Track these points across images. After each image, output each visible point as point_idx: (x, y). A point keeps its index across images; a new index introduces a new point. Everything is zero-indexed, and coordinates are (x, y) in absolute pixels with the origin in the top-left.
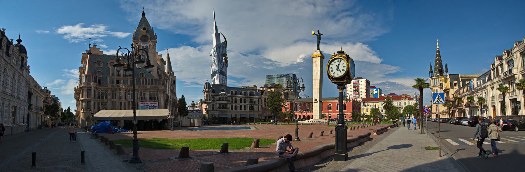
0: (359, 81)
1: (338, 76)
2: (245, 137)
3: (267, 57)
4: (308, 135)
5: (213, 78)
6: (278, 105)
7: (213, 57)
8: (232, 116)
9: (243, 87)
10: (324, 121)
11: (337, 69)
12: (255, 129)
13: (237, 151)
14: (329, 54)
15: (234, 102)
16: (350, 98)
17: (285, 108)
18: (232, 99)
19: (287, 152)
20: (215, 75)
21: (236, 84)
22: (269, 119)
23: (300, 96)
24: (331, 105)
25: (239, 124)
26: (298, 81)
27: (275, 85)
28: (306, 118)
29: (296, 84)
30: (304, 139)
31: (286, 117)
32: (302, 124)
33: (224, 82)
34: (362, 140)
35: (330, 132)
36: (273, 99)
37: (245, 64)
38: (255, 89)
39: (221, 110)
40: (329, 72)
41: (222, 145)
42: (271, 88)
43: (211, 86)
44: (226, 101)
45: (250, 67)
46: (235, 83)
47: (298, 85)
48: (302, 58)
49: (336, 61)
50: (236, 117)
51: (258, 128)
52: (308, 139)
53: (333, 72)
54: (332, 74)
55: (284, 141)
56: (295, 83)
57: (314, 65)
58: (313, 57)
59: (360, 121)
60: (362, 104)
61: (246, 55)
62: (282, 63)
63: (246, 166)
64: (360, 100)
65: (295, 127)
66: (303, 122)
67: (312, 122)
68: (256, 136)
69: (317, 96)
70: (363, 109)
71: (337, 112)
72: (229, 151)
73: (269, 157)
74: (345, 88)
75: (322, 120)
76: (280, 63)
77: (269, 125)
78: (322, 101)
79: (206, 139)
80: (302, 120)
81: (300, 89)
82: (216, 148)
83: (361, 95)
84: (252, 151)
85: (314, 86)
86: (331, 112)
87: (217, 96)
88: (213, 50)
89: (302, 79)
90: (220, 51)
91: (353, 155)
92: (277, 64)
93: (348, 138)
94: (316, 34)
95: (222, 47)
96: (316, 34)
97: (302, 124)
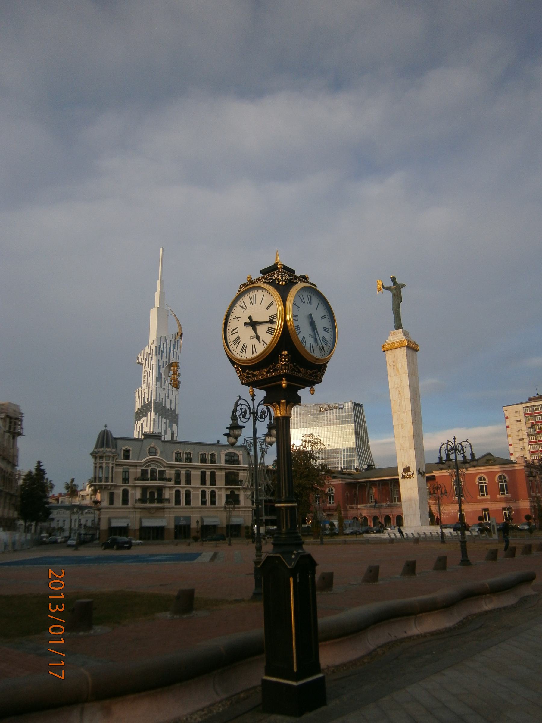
5: (140, 422)
18: (178, 475)
39: (148, 505)
57: (390, 371)
90: (164, 354)
95: (168, 346)
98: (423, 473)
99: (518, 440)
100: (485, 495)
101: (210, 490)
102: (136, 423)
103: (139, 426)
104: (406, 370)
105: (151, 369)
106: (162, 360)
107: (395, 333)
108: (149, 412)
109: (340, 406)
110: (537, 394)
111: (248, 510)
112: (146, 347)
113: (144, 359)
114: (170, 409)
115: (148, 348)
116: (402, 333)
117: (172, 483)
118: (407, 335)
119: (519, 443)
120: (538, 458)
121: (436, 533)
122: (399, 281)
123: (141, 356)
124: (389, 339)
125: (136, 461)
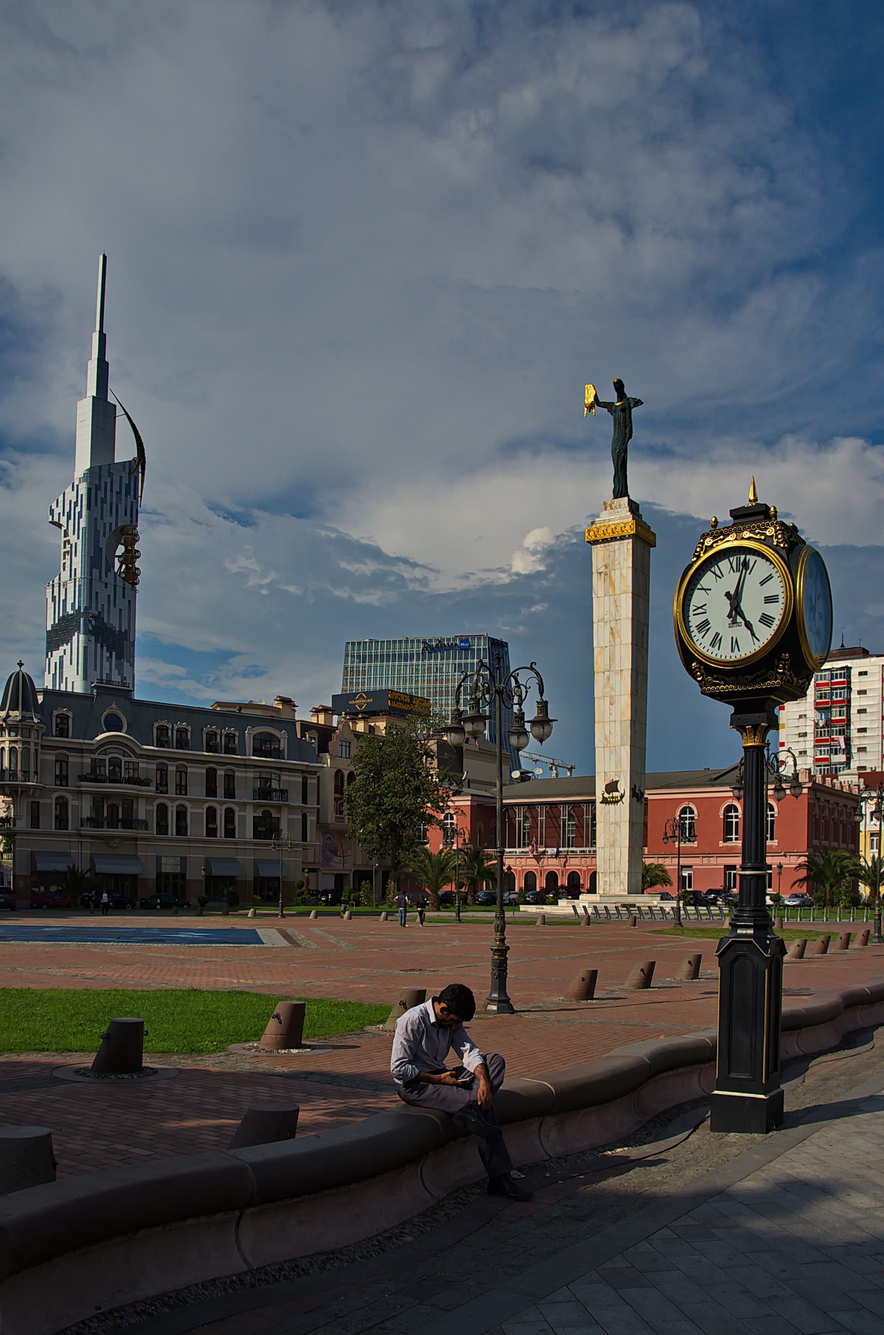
0: (849, 669)
1: (736, 656)
2: (229, 987)
3: (356, 534)
4: (575, 984)
5: (57, 654)
6: (408, 811)
7: (66, 534)
8: (165, 869)
9: (219, 704)
10: (656, 902)
11: (729, 616)
12: (285, 943)
13: (187, 1063)
14: (686, 518)
15: (172, 787)
16: (796, 775)
17: (442, 832)
18: (162, 771)
19: (443, 1075)
20: (68, 640)
21: (183, 685)
22: (357, 888)
23: (525, 766)
24: (692, 812)
25: (201, 915)
26: (517, 682)
27: (395, 696)
28: (562, 887)
29: (501, 699)
30: (552, 1007)
31: (448, 880)
32: (539, 923)
33: (120, 673)
34: (861, 1018)
35: (685, 968)
36: (378, 776)
37: (234, 568)
38: (284, 716)
40: (689, 633)
41: (104, 1029)
42: (370, 714)
43: (40, 698)
44: (128, 781)
45: (261, 587)
46: (179, 678)
47: (516, 708)
48: (539, 549)
49: (724, 565)
50: (183, 875)
51: (300, 937)
52: (574, 1004)
53: (710, 636)
54: (702, 644)
55: (433, 1019)
56: (499, 692)
57: (598, 585)
58: (596, 542)
59: (855, 901)
60: (862, 786)
61: (242, 519)
62: (438, 572)
63: (231, 1147)
64: (855, 779)
65: (491, 941)
66: (547, 909)
67: (590, 911)
68: (288, 982)
69: (618, 763)
70: (872, 835)
71: (729, 852)
72: (148, 1061)
73: (355, 1102)
74: (774, 724)
75: (644, 900)
76: (426, 573)
77: (355, 919)
78: (642, 794)
79: (22, 993)
80: (540, 900)
81: (525, 733)
82: (75, 1043)
83: (862, 750)
84: (264, 1066)
85: (601, 707)
86: (692, 854)
87: (82, 751)
88: (71, 495)
89: (537, 674)
90: (107, 507)
91: (809, 1102)
92: (408, 573)
93: (788, 1005)
94: (605, 405)
96: (605, 405)
97: (539, 923)
98: (639, 794)
99: (796, 734)
100: (734, 839)
101: (177, 803)
102: (49, 656)
103: (56, 663)
104: (629, 586)
105: (78, 538)
106: (102, 518)
107: (613, 506)
108: (76, 633)
109: (463, 644)
110: (842, 646)
111: (254, 849)
112: (69, 488)
113: (64, 515)
114: (117, 629)
115: (73, 490)
116: (627, 505)
117: (151, 790)
118: (635, 512)
119: (798, 742)
120: (826, 773)
121: (647, 908)
122: (629, 393)
123: (57, 506)
124: (601, 516)
125: (82, 741)
